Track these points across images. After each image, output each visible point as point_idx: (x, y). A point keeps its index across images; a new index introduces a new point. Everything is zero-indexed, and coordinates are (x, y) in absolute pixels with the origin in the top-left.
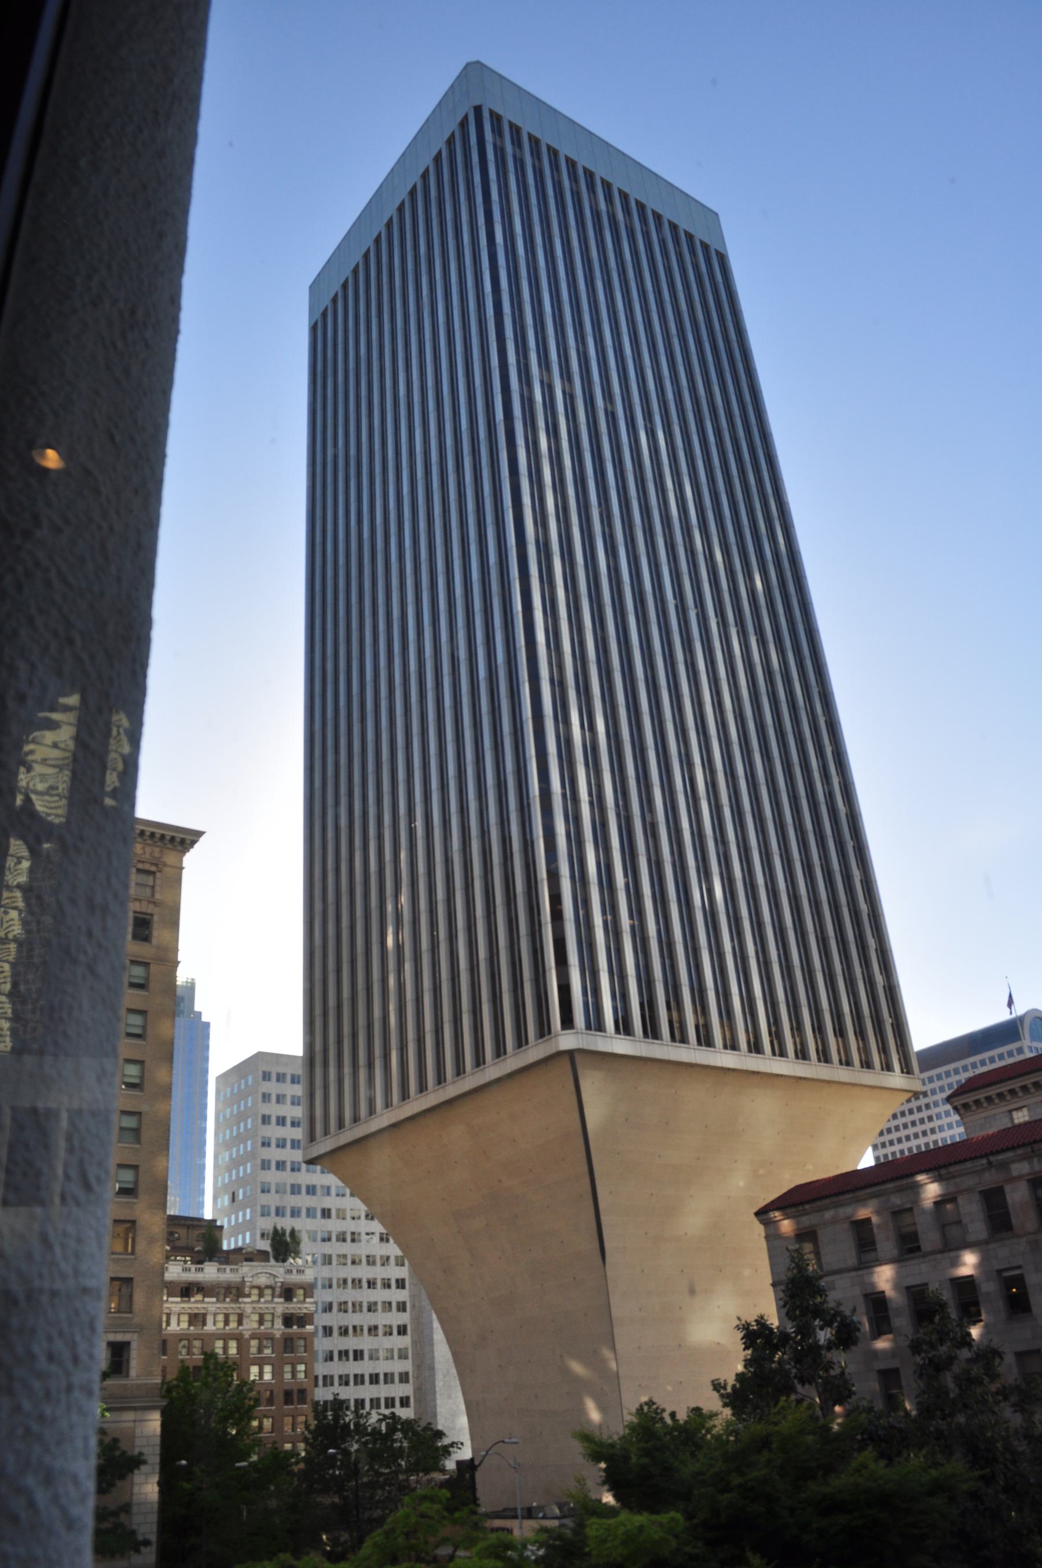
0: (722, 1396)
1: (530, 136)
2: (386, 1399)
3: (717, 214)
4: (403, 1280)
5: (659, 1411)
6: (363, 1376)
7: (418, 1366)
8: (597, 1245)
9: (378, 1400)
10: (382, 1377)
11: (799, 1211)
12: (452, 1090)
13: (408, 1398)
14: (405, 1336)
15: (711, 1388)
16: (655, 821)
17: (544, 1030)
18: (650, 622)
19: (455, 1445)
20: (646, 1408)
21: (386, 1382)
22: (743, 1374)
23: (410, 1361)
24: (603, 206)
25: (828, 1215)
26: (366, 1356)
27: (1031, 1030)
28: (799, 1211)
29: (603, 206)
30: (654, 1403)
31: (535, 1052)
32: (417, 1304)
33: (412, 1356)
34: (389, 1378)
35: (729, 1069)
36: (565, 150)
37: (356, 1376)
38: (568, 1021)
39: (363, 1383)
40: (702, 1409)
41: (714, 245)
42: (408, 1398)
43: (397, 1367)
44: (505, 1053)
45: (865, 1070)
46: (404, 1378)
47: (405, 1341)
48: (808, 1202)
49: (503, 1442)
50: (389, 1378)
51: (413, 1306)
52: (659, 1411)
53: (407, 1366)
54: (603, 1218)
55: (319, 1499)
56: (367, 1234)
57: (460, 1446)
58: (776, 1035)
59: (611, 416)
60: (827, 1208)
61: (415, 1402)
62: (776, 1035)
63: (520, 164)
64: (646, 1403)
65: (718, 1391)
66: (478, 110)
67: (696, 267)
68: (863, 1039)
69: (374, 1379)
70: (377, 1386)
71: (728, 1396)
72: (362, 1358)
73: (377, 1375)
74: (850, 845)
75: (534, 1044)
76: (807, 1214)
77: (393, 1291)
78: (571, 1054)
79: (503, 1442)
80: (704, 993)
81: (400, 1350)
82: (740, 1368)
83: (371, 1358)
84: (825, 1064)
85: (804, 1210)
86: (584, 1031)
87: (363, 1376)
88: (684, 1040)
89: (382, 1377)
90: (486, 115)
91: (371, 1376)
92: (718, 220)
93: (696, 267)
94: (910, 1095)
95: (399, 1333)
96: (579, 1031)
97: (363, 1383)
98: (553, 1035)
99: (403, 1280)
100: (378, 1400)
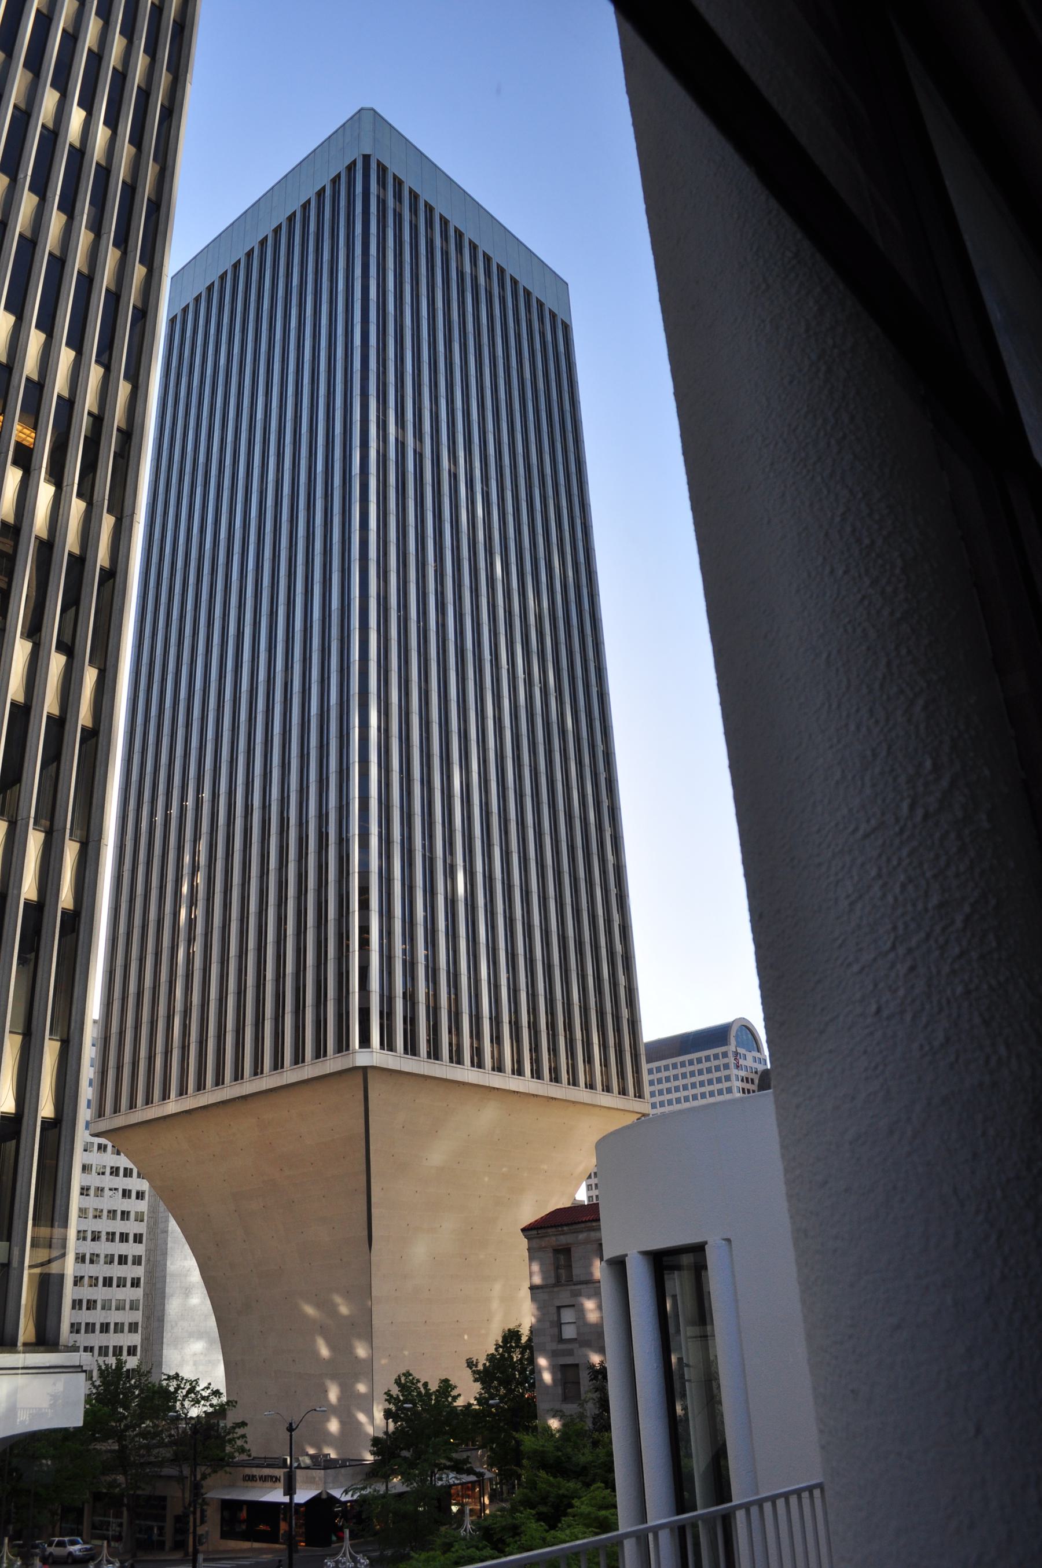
0: (474, 1372)
1: (411, 191)
2: (115, 1347)
3: (567, 284)
4: (141, 1235)
5: (415, 1381)
6: (94, 1324)
7: (147, 1317)
8: (366, 1233)
9: (107, 1347)
10: (112, 1327)
11: (559, 1231)
12: (250, 1086)
13: (135, 1347)
14: (138, 1289)
15: (466, 1365)
16: (454, 864)
17: (343, 1045)
18: (487, 717)
19: (230, 1404)
20: (403, 1379)
21: (115, 1332)
22: (492, 1354)
23: (140, 1312)
24: (467, 269)
25: (582, 1236)
26: (99, 1306)
27: (737, 1037)
28: (559, 1231)
29: (467, 269)
30: (411, 1375)
31: (333, 1064)
32: (151, 1259)
33: (143, 1309)
34: (119, 1328)
35: (494, 1088)
36: (441, 208)
37: (87, 1324)
38: (365, 1041)
39: (93, 1331)
40: (450, 1381)
41: (561, 316)
42: (135, 1347)
43: (126, 1317)
44: (303, 1061)
45: (605, 1093)
46: (133, 1327)
47: (138, 1293)
48: (567, 1225)
49: (315, 1410)
50: (119, 1328)
51: (148, 1260)
52: (415, 1381)
53: (138, 1316)
54: (374, 1211)
55: (98, 1447)
56: (111, 1189)
57: (235, 1404)
58: (536, 1062)
59: (454, 477)
60: (581, 1232)
61: (142, 1351)
62: (536, 1062)
63: (398, 217)
64: (404, 1374)
65: (471, 1368)
66: (366, 158)
67: (543, 335)
68: (606, 1066)
69: (105, 1328)
70: (107, 1334)
71: (478, 1372)
72: (95, 1308)
73: (108, 1324)
74: (613, 891)
75: (332, 1057)
76: (563, 1234)
77: (131, 1246)
78: (365, 1070)
79: (315, 1410)
80: (480, 1020)
81: (132, 1302)
82: (492, 1350)
83: (103, 1308)
84: (573, 1087)
85: (563, 1231)
86: (379, 1051)
87: (94, 1324)
88: (460, 1061)
89: (112, 1327)
90: (374, 166)
91: (102, 1324)
92: (568, 288)
93: (543, 335)
94: (640, 1115)
95: (132, 1285)
96: (374, 1050)
97: (93, 1331)
98: (351, 1052)
99: (141, 1235)
100: (107, 1347)
